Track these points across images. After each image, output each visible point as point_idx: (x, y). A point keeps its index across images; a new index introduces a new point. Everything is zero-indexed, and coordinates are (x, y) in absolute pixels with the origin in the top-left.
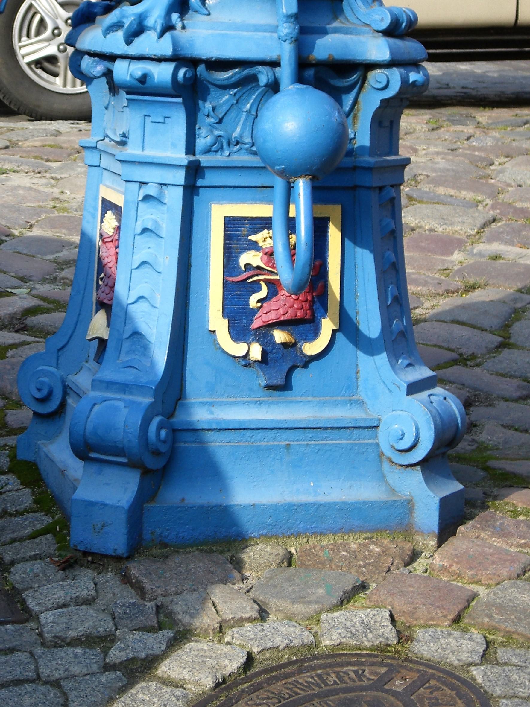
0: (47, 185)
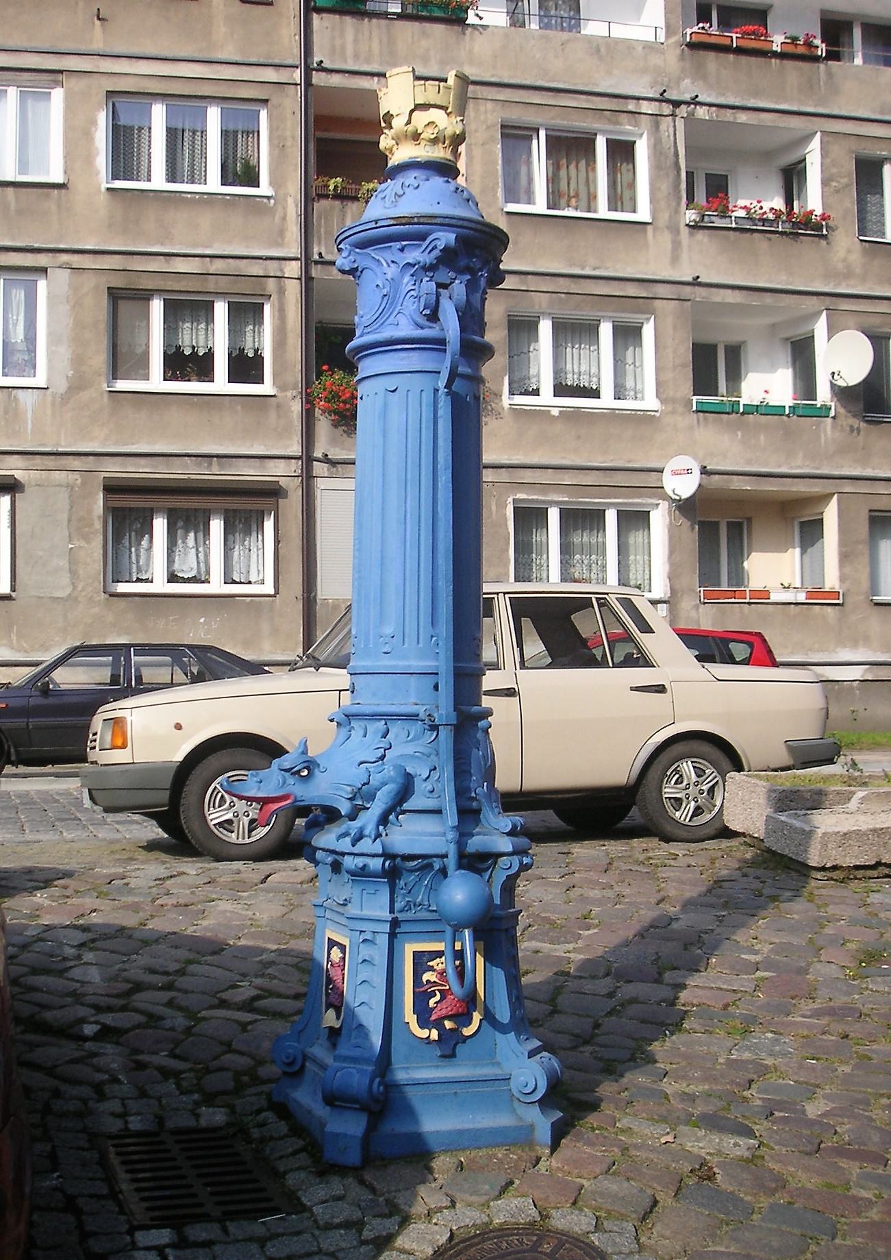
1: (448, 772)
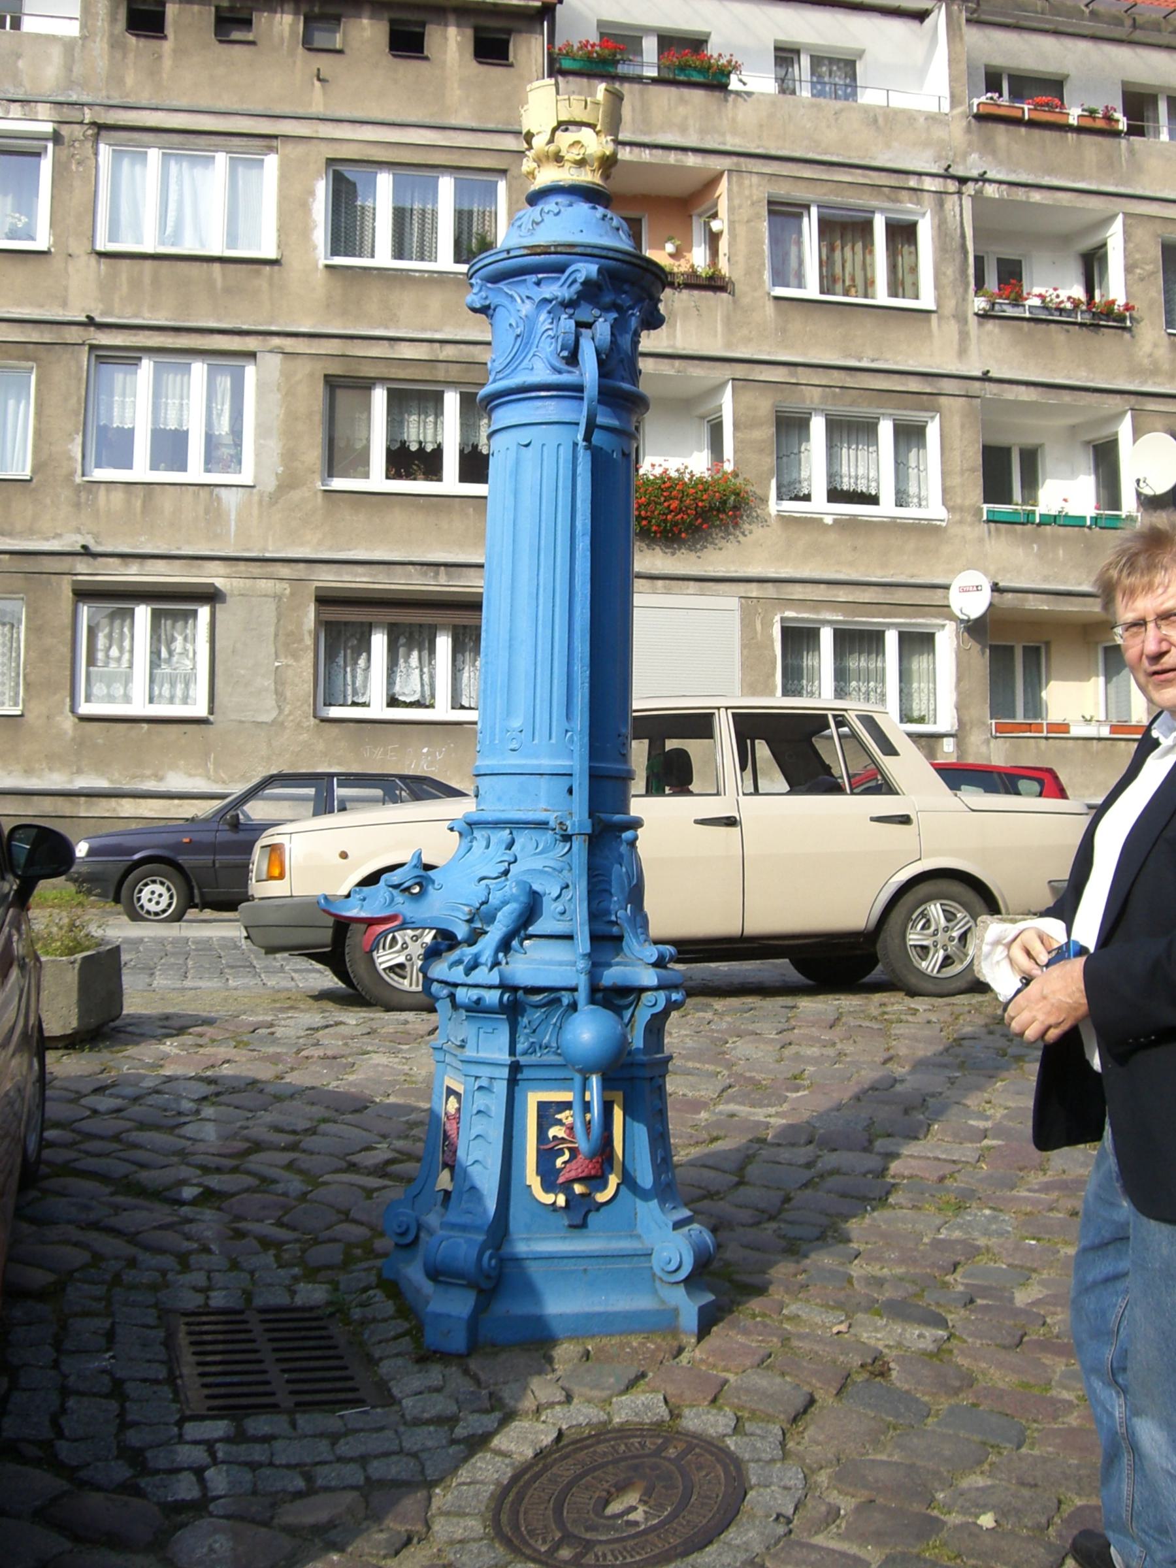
0: (399, 1063)
1: (580, 889)
